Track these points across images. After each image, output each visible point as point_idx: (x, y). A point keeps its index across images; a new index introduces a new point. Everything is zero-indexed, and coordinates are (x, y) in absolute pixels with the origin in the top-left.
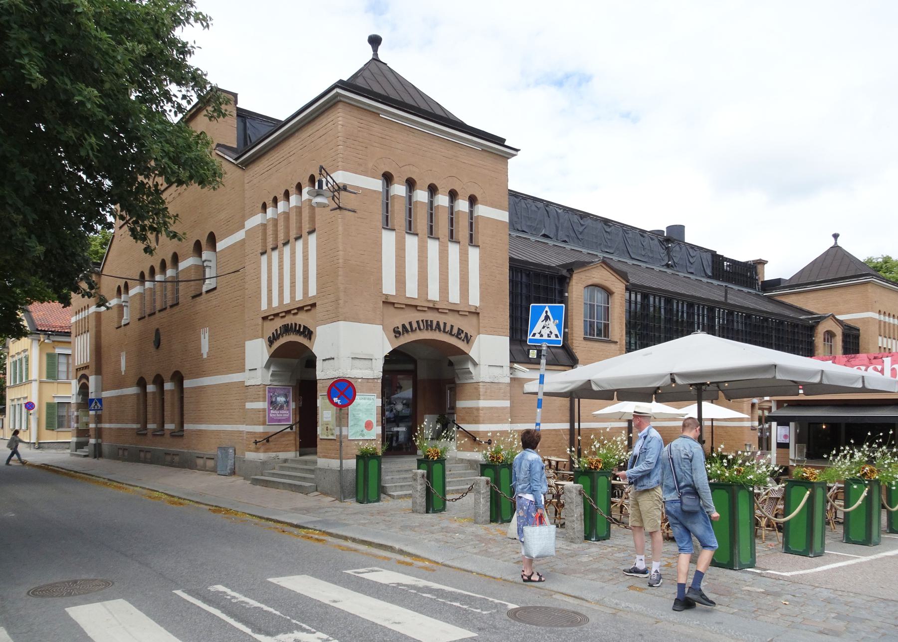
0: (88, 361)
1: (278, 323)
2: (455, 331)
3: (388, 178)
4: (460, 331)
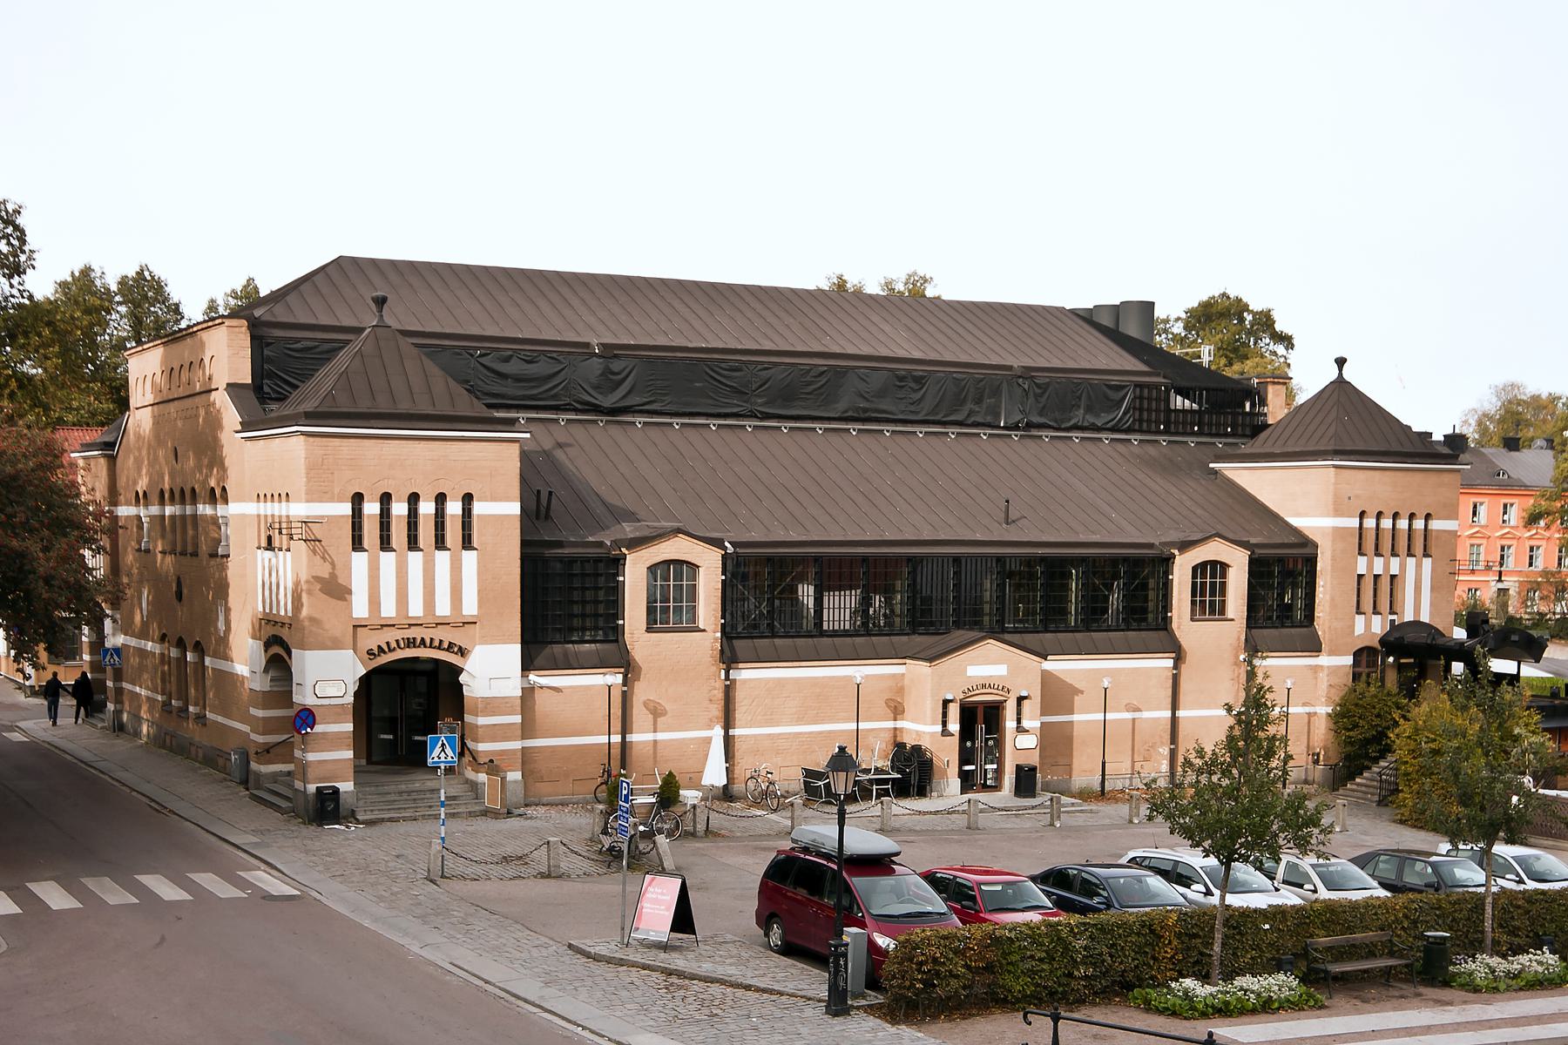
2: (446, 645)
4: (451, 645)
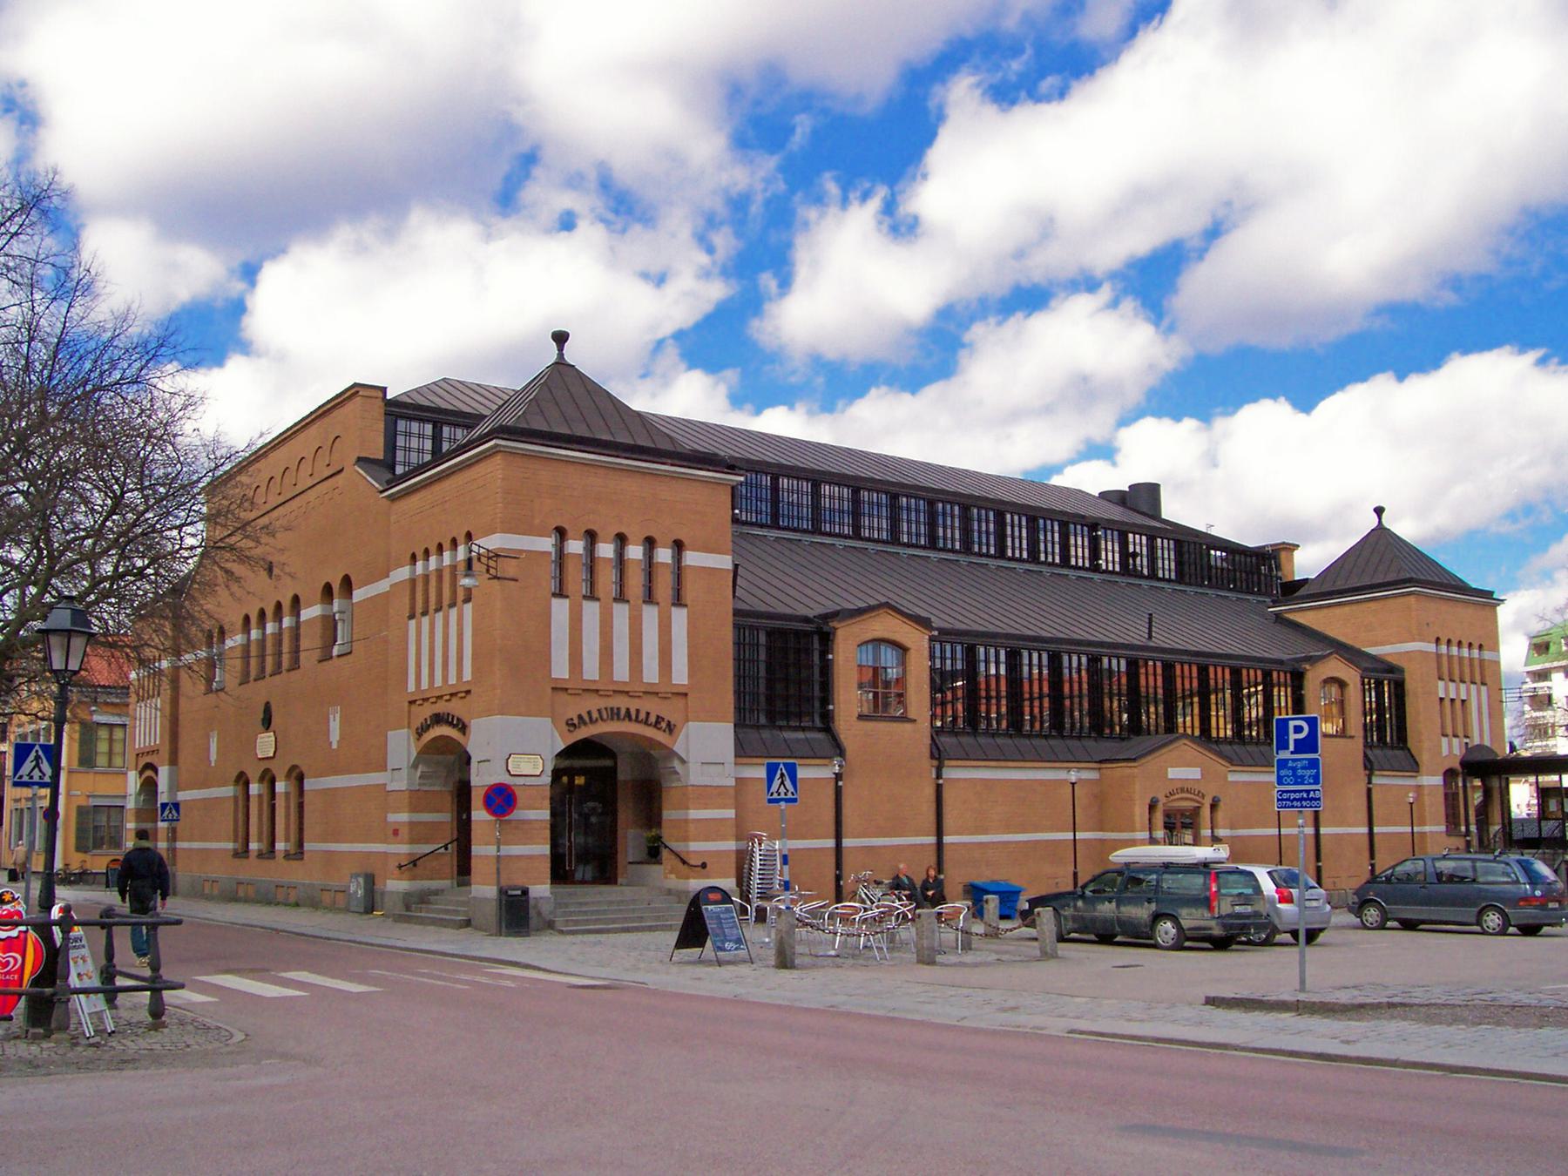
0: (158, 742)
1: (427, 711)
2: (653, 719)
3: (561, 533)
4: (659, 719)
